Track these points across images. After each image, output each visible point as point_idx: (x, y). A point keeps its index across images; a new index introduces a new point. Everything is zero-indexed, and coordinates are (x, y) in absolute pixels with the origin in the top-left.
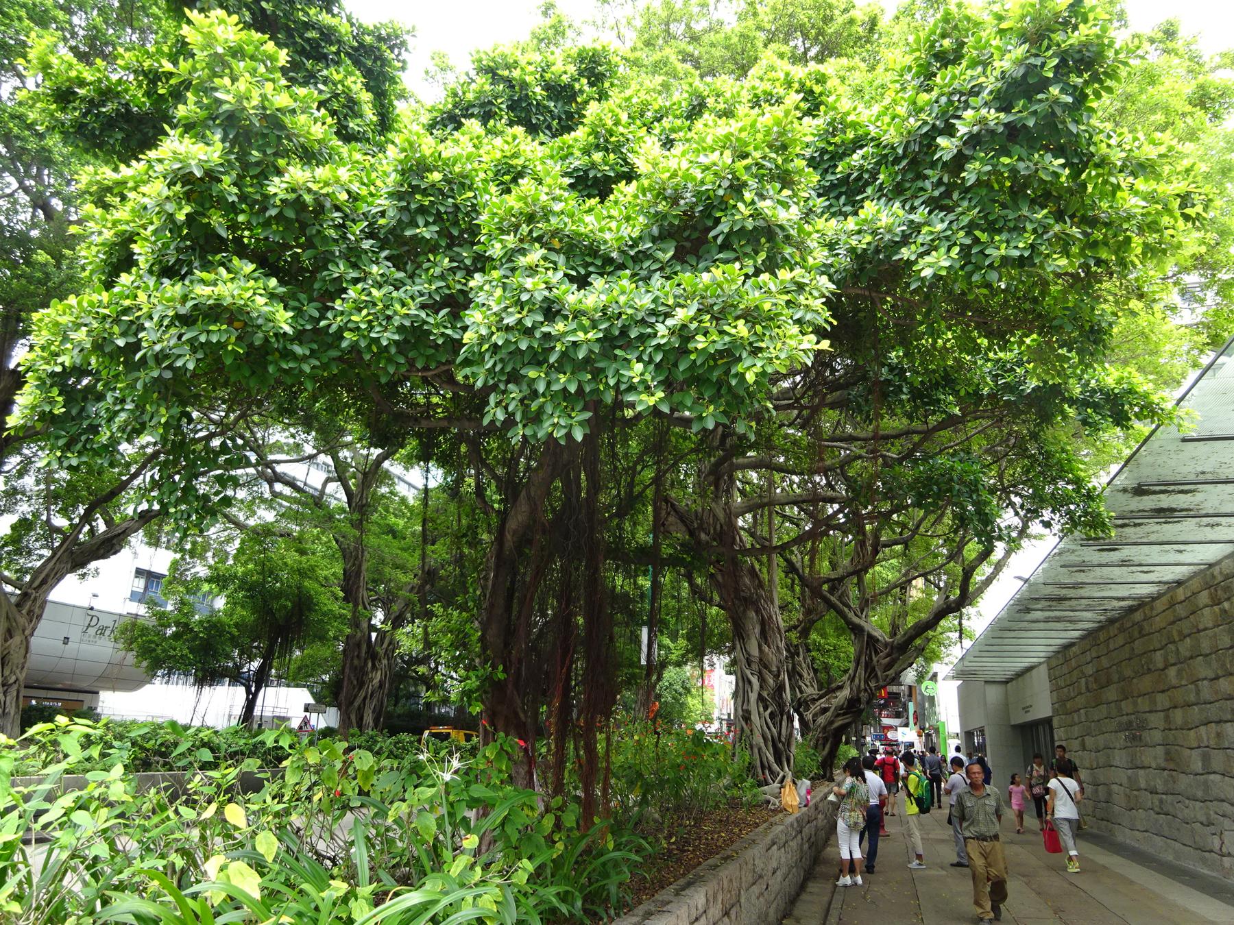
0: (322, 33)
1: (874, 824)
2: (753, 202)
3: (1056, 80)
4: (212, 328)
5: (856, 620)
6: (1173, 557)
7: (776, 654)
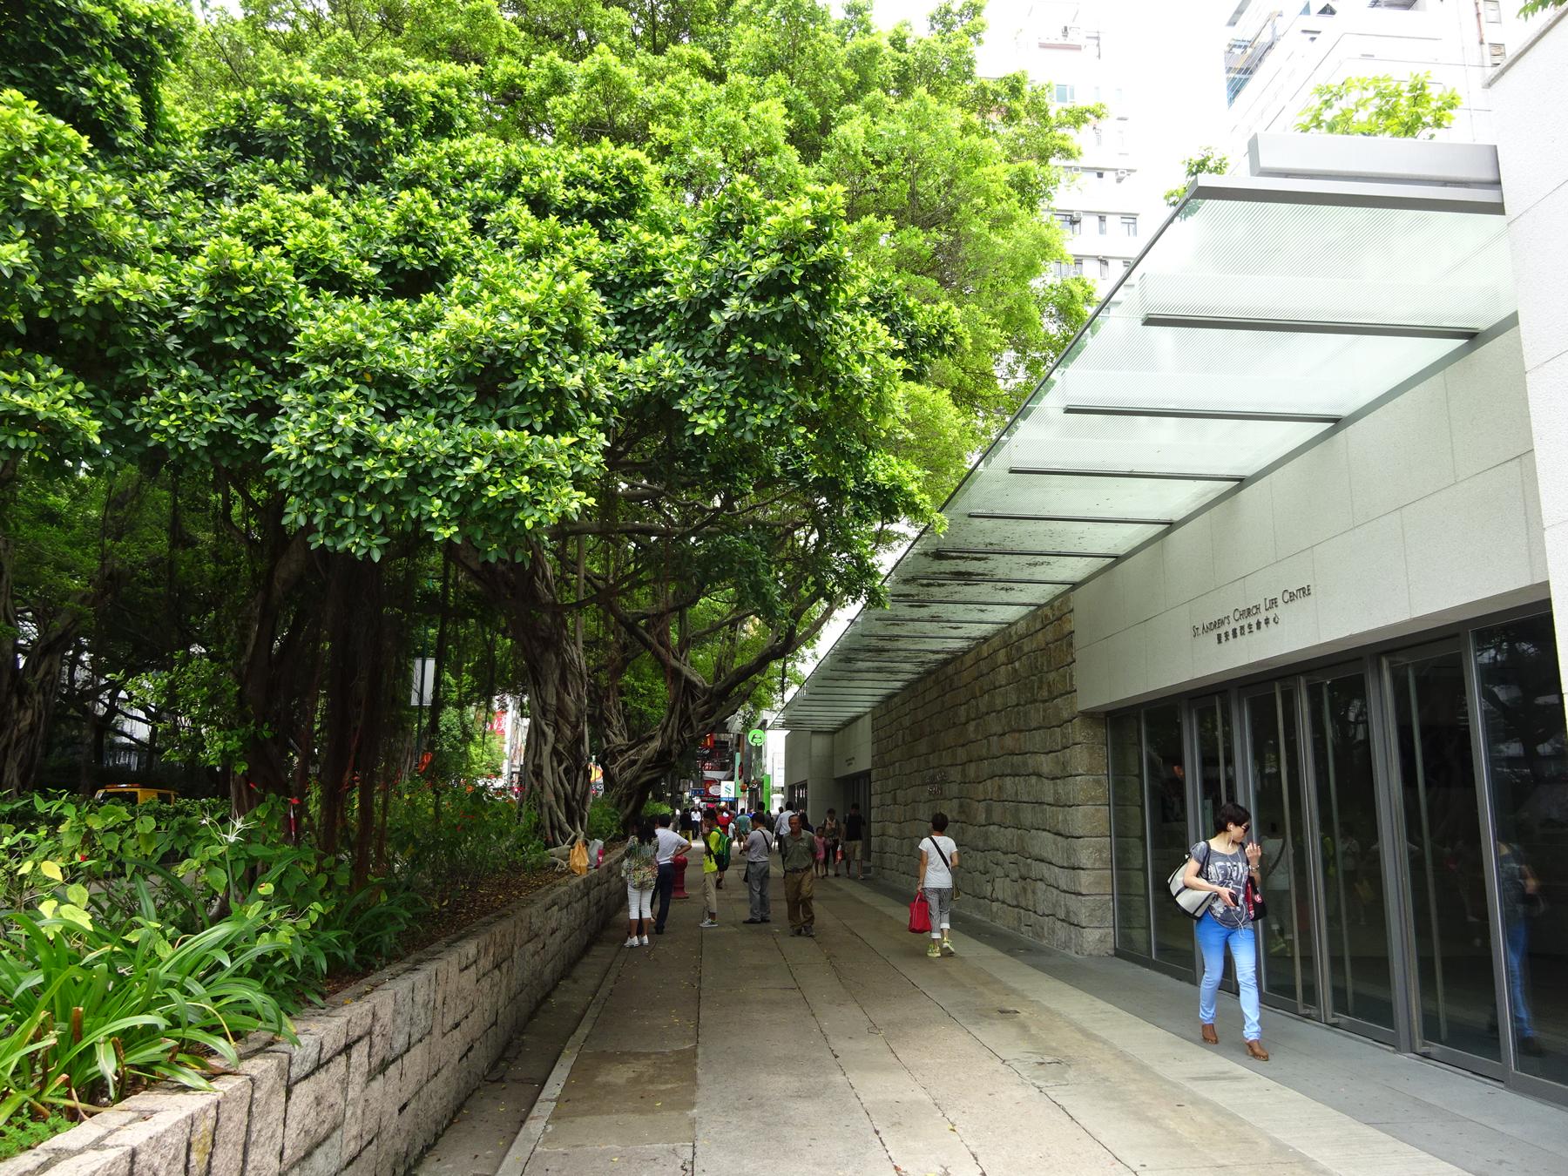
0: (81, 21)
1: (670, 881)
2: (546, 367)
3: (801, 287)
4: (21, 434)
5: (674, 663)
6: (977, 616)
7: (575, 700)
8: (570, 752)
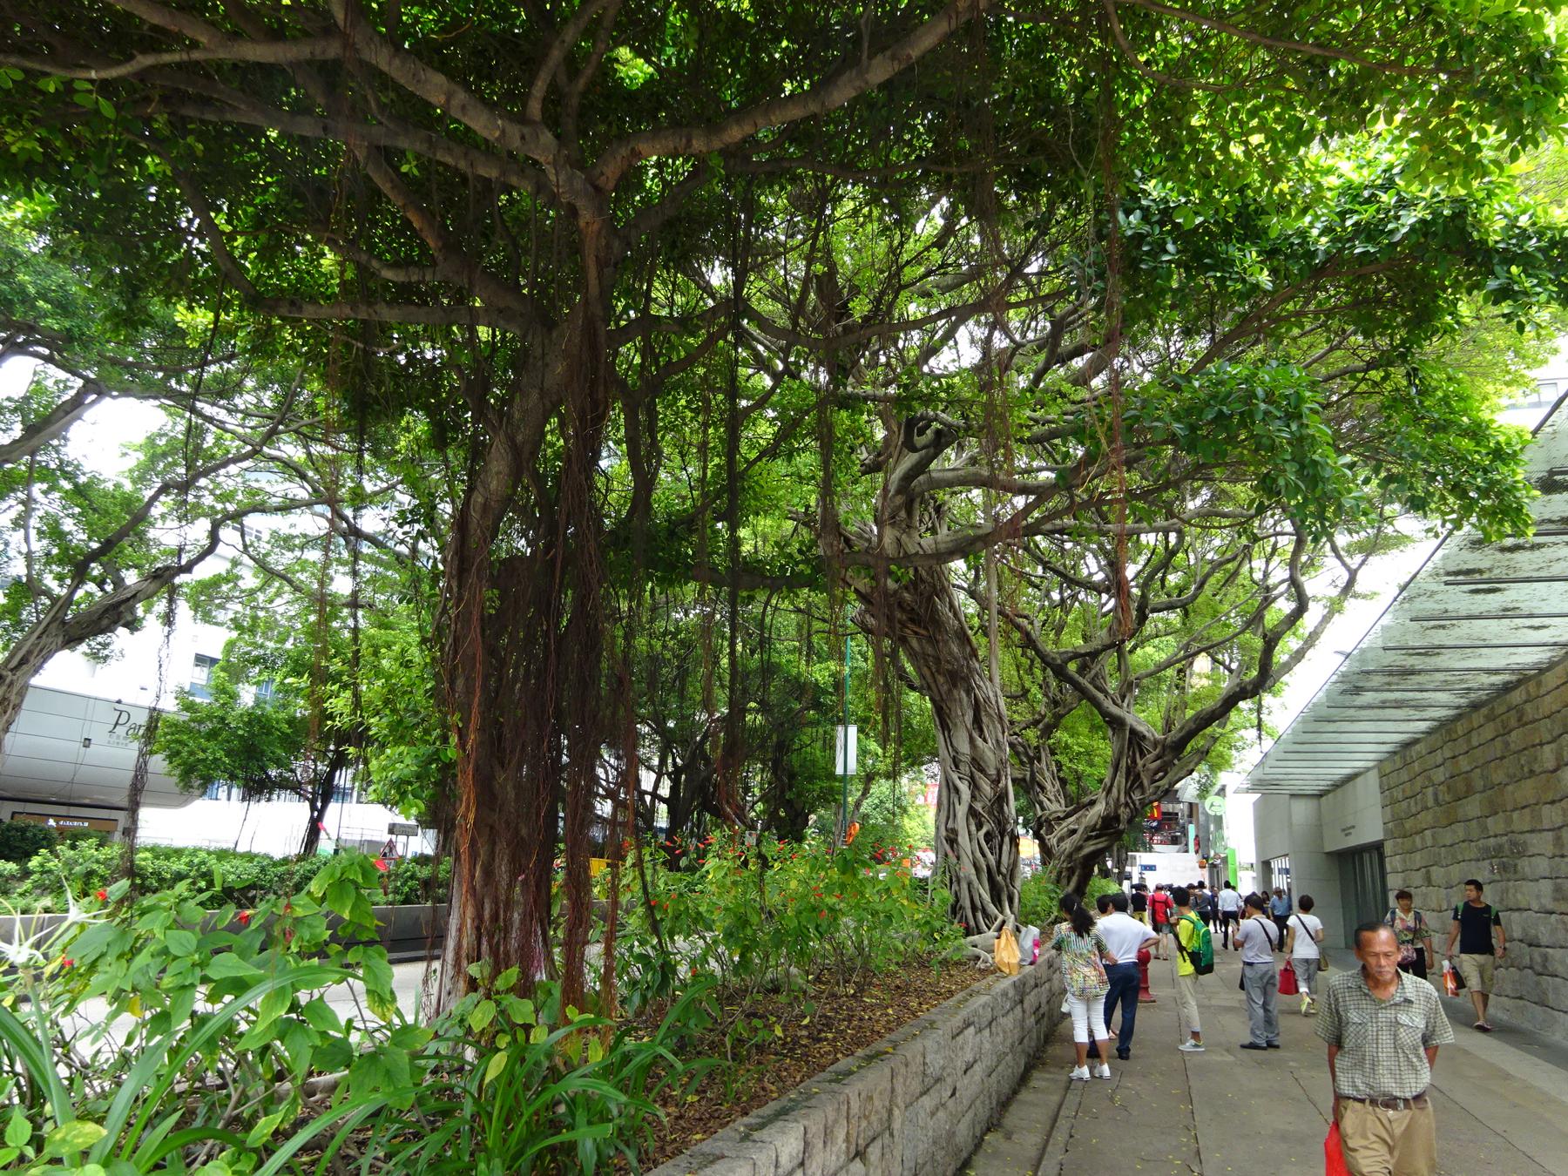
1: (1126, 986)
5: (1114, 710)
8: (990, 813)
